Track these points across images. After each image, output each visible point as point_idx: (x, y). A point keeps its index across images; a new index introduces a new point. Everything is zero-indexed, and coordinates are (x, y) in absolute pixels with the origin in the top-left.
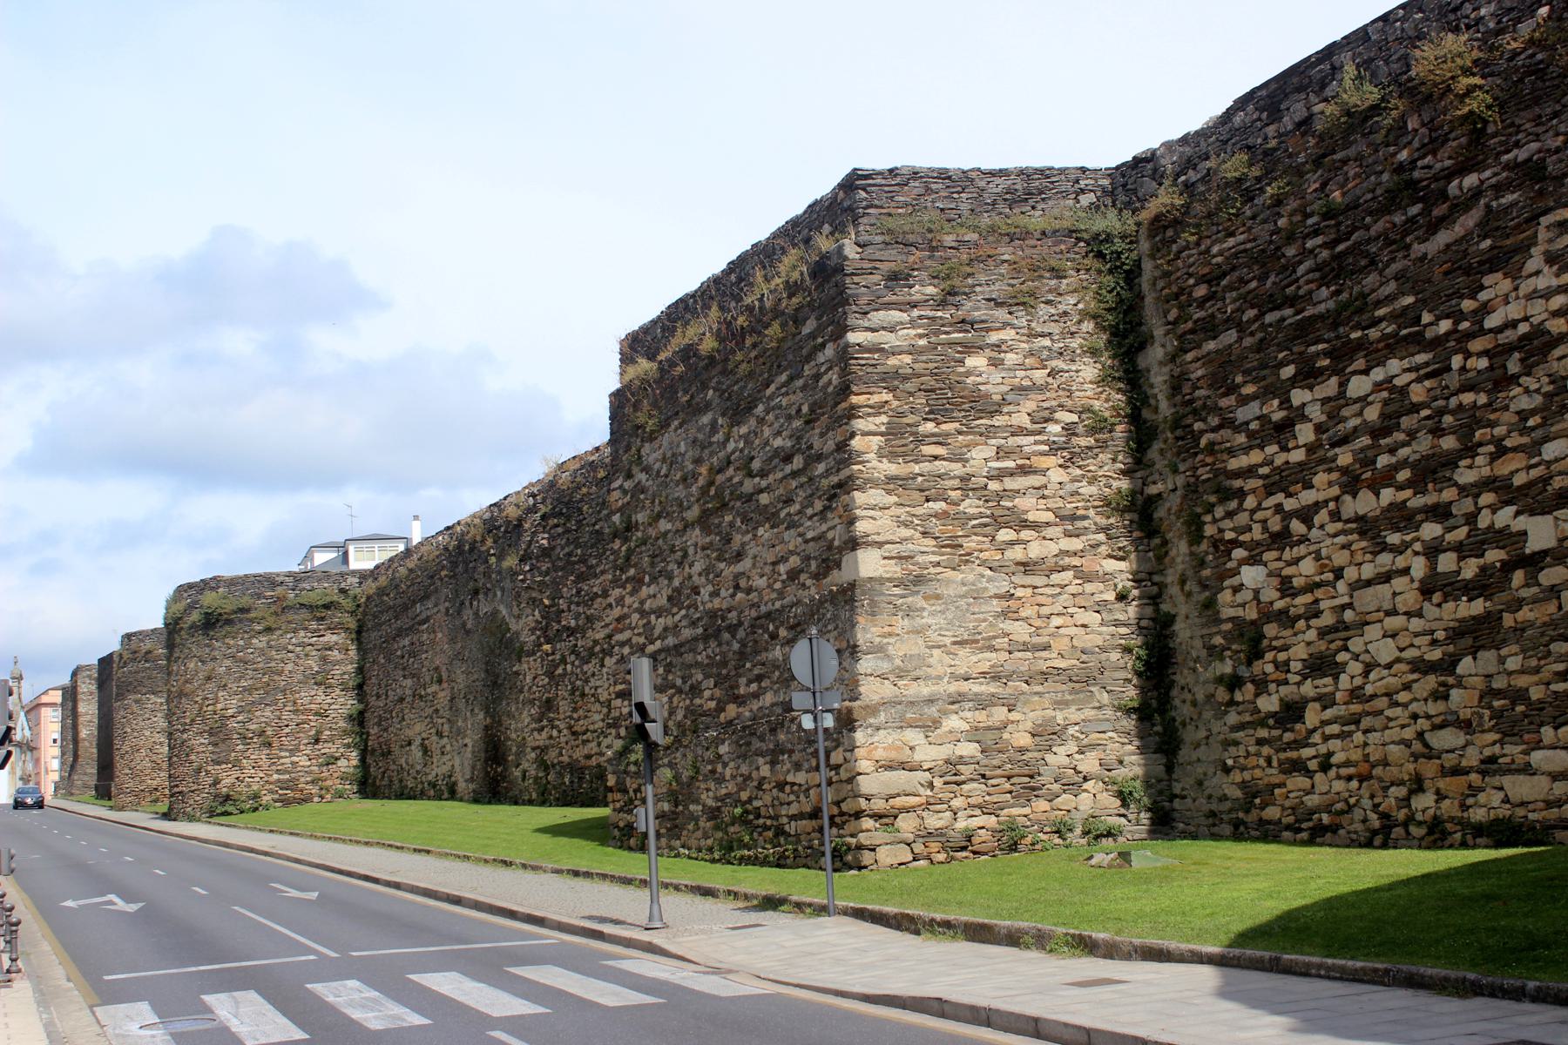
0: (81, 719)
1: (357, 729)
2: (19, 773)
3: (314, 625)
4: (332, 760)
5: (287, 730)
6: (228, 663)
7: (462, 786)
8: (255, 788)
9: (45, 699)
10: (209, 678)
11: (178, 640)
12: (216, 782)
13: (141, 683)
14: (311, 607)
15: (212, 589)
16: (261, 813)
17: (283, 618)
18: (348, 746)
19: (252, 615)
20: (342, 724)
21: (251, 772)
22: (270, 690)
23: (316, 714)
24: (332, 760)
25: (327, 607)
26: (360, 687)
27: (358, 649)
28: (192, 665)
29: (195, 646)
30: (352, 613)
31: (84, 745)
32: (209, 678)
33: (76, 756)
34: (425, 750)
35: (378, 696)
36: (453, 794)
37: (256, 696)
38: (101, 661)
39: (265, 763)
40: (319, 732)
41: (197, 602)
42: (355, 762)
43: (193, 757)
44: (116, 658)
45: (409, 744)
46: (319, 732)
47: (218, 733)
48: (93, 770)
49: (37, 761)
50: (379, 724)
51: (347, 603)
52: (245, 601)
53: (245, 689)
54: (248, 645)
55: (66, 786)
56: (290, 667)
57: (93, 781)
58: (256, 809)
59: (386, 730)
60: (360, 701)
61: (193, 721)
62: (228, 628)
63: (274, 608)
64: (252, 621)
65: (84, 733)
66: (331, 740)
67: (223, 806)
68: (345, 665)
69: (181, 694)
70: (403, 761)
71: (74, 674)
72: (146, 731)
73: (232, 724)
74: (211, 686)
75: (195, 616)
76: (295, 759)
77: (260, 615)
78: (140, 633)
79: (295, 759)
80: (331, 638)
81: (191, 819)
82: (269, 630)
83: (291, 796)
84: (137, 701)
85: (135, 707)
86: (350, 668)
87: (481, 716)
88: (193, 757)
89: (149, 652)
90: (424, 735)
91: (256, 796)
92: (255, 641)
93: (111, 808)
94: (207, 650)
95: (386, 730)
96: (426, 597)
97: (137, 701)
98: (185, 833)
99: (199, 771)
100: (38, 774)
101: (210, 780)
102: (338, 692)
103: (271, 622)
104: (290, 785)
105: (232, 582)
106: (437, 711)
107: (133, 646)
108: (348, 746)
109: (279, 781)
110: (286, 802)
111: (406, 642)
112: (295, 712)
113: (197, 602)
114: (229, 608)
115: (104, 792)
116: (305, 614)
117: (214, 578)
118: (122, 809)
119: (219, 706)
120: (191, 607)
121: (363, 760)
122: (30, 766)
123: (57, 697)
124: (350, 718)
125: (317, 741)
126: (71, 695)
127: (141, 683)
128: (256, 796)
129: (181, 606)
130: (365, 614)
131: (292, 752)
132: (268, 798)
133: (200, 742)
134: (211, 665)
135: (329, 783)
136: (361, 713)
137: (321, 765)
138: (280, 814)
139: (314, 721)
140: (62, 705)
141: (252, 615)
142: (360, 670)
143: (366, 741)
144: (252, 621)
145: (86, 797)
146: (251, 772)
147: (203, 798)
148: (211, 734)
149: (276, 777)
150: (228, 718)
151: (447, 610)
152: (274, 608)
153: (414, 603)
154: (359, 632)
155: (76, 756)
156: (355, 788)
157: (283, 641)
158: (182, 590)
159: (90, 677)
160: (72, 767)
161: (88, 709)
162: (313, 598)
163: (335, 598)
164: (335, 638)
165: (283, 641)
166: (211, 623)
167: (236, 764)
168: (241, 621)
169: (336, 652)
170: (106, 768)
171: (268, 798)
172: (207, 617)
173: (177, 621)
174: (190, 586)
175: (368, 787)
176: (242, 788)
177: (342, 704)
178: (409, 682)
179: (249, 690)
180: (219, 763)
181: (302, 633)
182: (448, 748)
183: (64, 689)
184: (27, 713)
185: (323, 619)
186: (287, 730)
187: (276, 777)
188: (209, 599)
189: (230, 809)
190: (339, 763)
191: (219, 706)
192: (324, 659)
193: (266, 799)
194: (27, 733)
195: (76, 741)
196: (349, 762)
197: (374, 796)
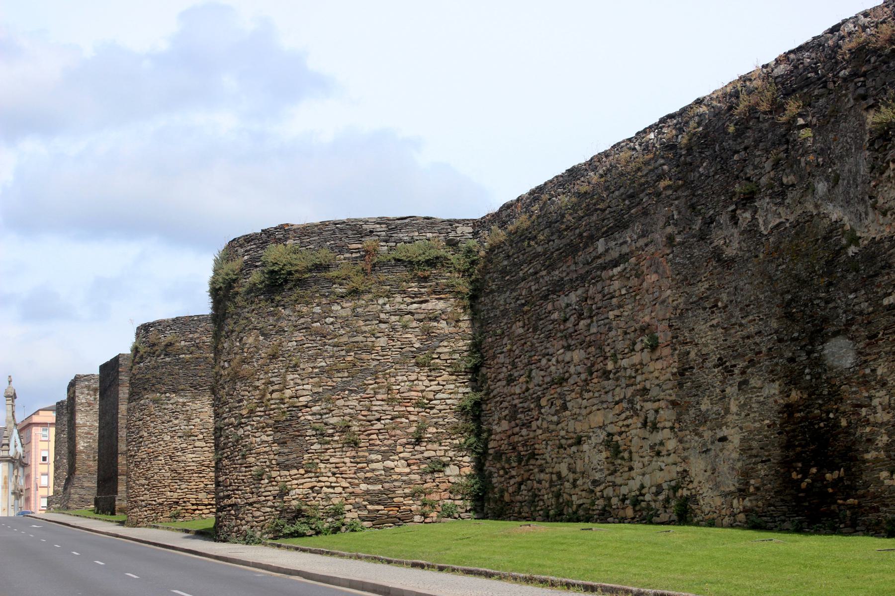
0: (79, 431)
1: (472, 426)
2: (11, 488)
3: (414, 287)
4: (437, 467)
5: (379, 425)
6: (299, 336)
7: (709, 500)
8: (336, 501)
9: (36, 419)
10: (273, 357)
11: (231, 309)
12: (283, 493)
13: (160, 380)
14: (410, 264)
15: (278, 241)
16: (345, 536)
17: (374, 277)
18: (459, 448)
19: (333, 273)
20: (452, 419)
21: (332, 480)
22: (357, 373)
23: (418, 404)
24: (437, 467)
25: (431, 263)
26: (475, 369)
27: (472, 320)
28: (251, 340)
29: (255, 315)
30: (465, 273)
31: (81, 457)
32: (273, 357)
33: (72, 470)
34: (613, 448)
35: (510, 380)
36: (684, 515)
37: (337, 379)
38: (103, 368)
39: (348, 467)
40: (422, 429)
41: (258, 259)
42: (467, 470)
43: (251, 459)
44: (125, 365)
45: (579, 442)
46: (422, 429)
47: (287, 428)
48: (91, 483)
49: (28, 477)
50: (513, 417)
51: (456, 259)
52: (324, 255)
53: (323, 371)
54: (327, 313)
55: (61, 500)
56: (383, 341)
57: (91, 495)
58: (336, 530)
59: (527, 425)
60: (476, 389)
61: (251, 412)
62: (299, 291)
63: (361, 264)
64: (332, 281)
65: (81, 445)
66: (437, 440)
67: (292, 524)
68: (455, 339)
69: (236, 377)
70: (563, 468)
71: (72, 385)
72: (180, 433)
73: (305, 416)
74: (277, 366)
75: (256, 276)
76: (389, 464)
77: (343, 273)
78: (159, 323)
79: (389, 464)
80: (436, 305)
81: (248, 540)
82: (355, 293)
83: (386, 513)
84: (155, 401)
85: (152, 407)
86: (462, 345)
87: (774, 389)
88: (251, 459)
89: (170, 344)
90: (611, 429)
91: (337, 512)
92: (336, 307)
93: (122, 523)
94: (271, 320)
95: (527, 425)
96: (622, 225)
97: (155, 401)
98: (265, 561)
99: (259, 477)
100: (28, 489)
101: (275, 490)
102: (446, 376)
103: (357, 281)
104: (383, 498)
105: (305, 232)
106: (645, 391)
107: (152, 337)
108: (459, 448)
109: (367, 492)
110: (377, 521)
111: (573, 297)
112: (390, 401)
113: (258, 259)
114: (302, 264)
115: (105, 505)
116: (402, 273)
117: (282, 227)
118: (136, 525)
119: (288, 393)
120: (249, 266)
121: (479, 466)
122: (22, 482)
123: (51, 417)
124: (462, 411)
125: (419, 441)
126: (66, 411)
127: (160, 380)
128: (337, 512)
129: (237, 264)
130: (485, 271)
131: (386, 456)
132: (354, 515)
133: (262, 439)
134: (276, 340)
135: (435, 497)
136: (477, 404)
137: (425, 473)
138: (369, 535)
139: (415, 415)
140: (56, 424)
141: (333, 273)
142: (476, 347)
143: (486, 442)
144: (332, 281)
145: (83, 511)
146: (332, 480)
147: (265, 512)
148: (276, 429)
149: (364, 487)
150: (300, 408)
151: (670, 239)
152: (361, 264)
153: (592, 239)
154: (473, 298)
155: (72, 470)
156: (469, 505)
157: (374, 308)
158: (234, 246)
159: (88, 387)
160: (68, 481)
161: (87, 421)
162: (414, 251)
163: (442, 252)
164: (441, 305)
165: (374, 308)
166: (278, 283)
167: (311, 469)
168: (316, 281)
169: (443, 324)
170: (108, 479)
171: (354, 515)
172: (267, 276)
173: (230, 284)
174: (248, 239)
175: (487, 502)
176: (317, 501)
177: (452, 393)
178: (577, 355)
179: (328, 372)
180: (287, 468)
181: (398, 298)
182: (671, 444)
183: (60, 405)
184: (20, 431)
185: (425, 279)
186: (379, 425)
187: (364, 487)
188: (274, 253)
189: (303, 528)
190: (448, 471)
191: (288, 393)
192: (428, 333)
193: (351, 516)
194: (20, 450)
195: (72, 453)
196: (459, 471)
197: (500, 515)
